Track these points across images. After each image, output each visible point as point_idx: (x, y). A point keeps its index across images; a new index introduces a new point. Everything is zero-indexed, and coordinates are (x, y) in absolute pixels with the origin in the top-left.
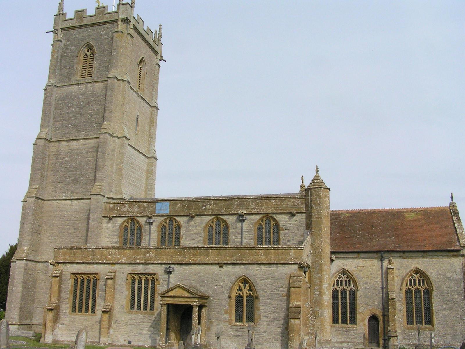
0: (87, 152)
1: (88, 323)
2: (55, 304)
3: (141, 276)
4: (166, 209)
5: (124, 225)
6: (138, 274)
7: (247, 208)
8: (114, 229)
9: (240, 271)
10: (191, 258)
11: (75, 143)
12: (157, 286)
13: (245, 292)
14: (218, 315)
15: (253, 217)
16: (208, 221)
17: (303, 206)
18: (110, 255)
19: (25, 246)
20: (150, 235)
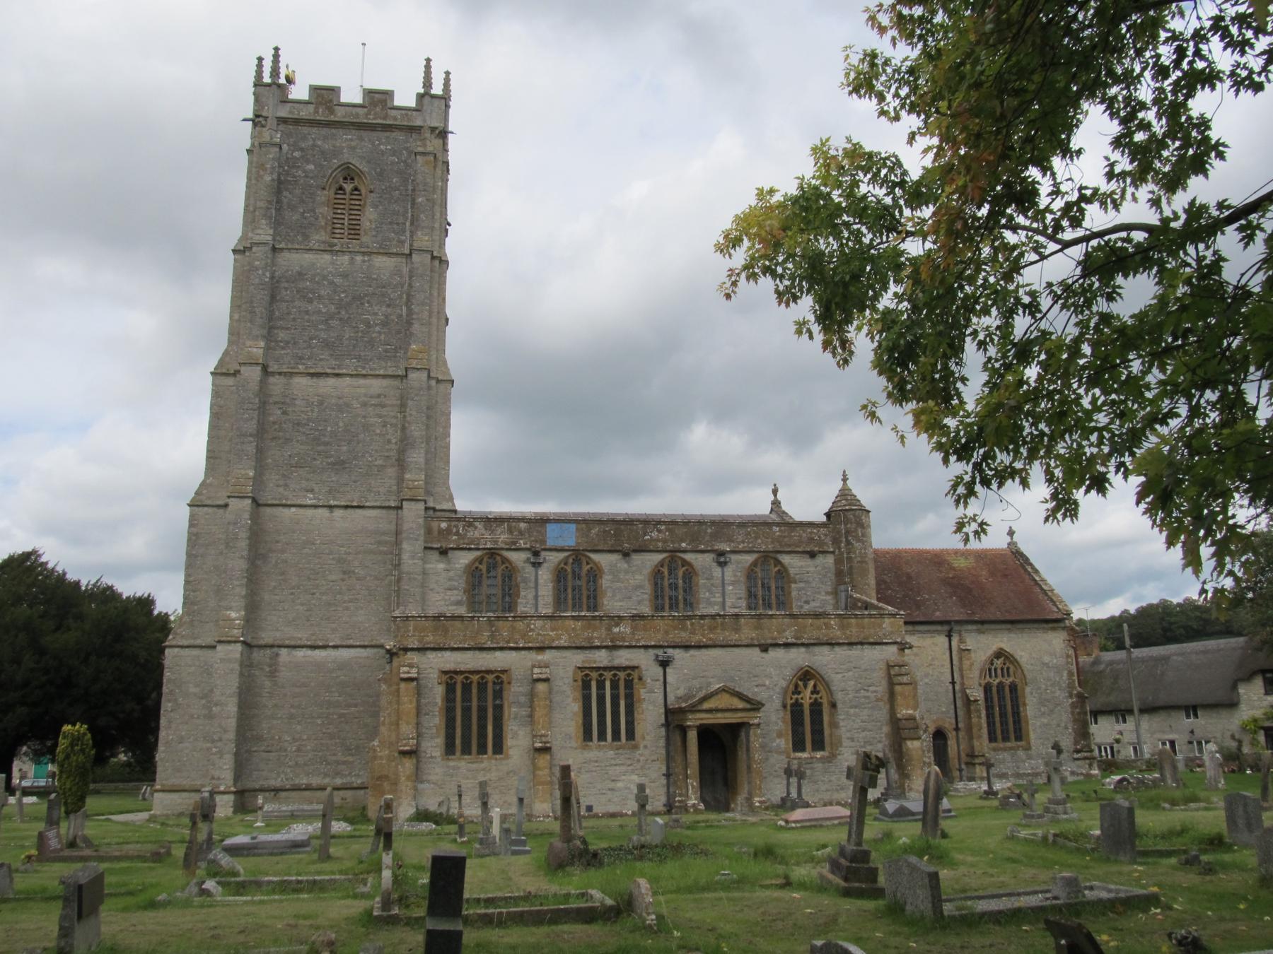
0: (364, 405)
4: (569, 537)
6: (598, 669)
7: (730, 540)
8: (451, 574)
9: (798, 657)
10: (717, 633)
11: (331, 381)
13: (807, 697)
17: (828, 540)
18: (531, 630)
19: (230, 609)
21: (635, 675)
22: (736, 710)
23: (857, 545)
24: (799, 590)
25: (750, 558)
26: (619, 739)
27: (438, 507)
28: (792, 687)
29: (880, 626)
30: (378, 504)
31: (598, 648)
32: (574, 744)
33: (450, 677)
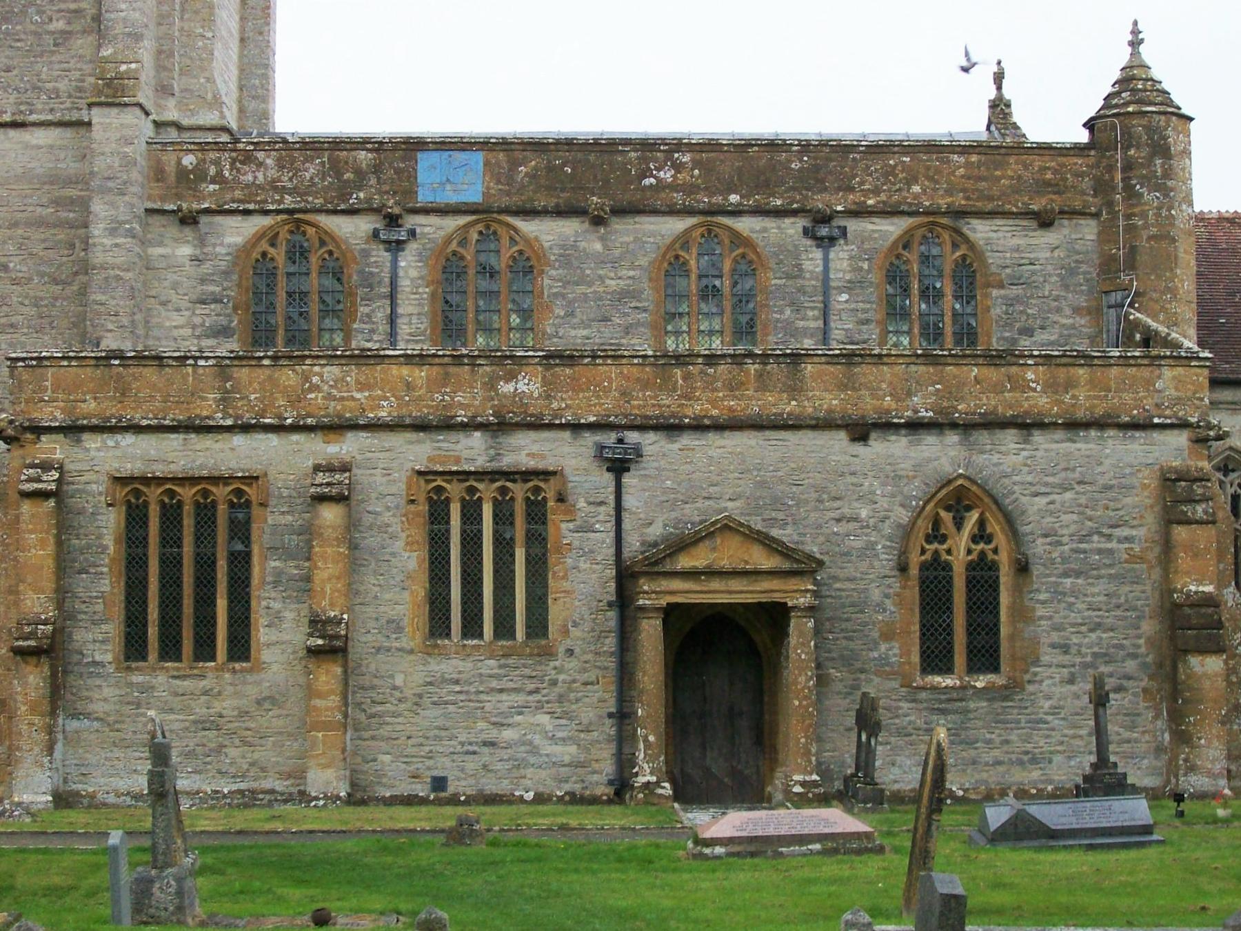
1: (217, 706)
2: (50, 627)
3: (480, 486)
5: (256, 255)
6: (464, 475)
8: (207, 268)
9: (942, 455)
12: (559, 529)
13: (959, 550)
14: (852, 645)
15: (871, 227)
16: (668, 241)
20: (392, 297)
21: (550, 490)
22: (756, 573)
23: (1148, 196)
24: (1010, 302)
25: (892, 228)
26: (511, 635)
27: (185, 122)
28: (924, 526)
29: (1149, 383)
30: (57, 116)
31: (464, 427)
32: (405, 643)
33: (132, 490)
